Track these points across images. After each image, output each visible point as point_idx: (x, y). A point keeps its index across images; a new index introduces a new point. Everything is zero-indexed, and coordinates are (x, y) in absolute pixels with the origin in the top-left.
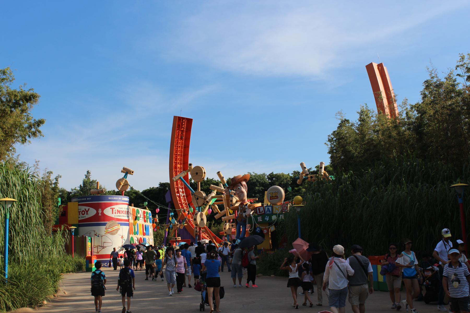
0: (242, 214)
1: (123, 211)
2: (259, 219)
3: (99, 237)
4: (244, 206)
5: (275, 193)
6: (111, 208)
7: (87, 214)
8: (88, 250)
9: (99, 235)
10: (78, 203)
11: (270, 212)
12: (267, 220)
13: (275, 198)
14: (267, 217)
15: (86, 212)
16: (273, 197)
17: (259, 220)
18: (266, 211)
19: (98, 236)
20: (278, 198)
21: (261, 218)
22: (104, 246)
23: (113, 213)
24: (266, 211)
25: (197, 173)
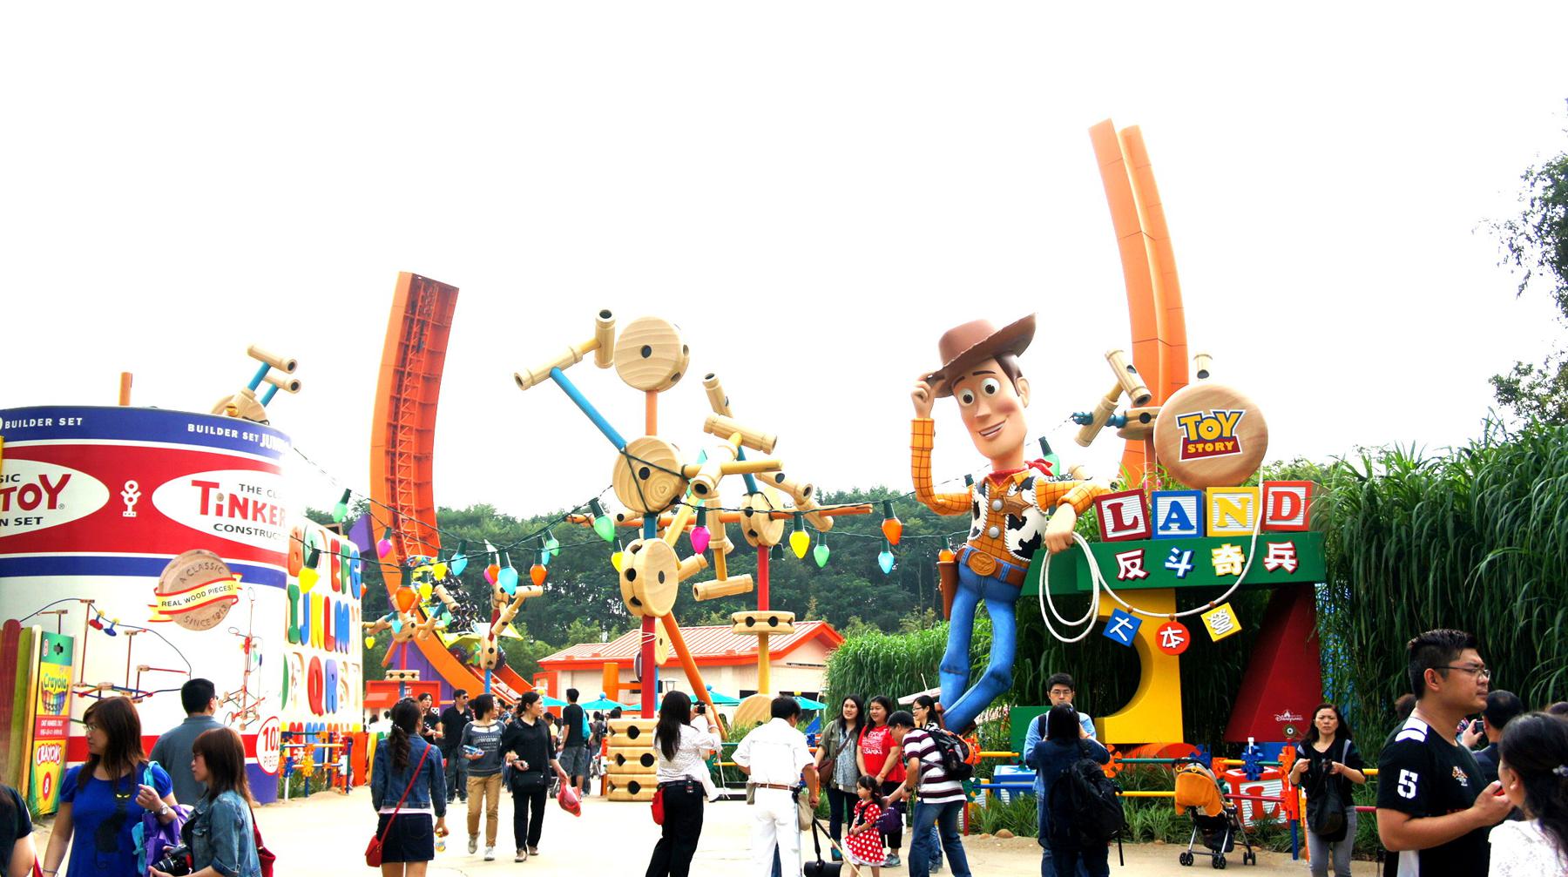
0: (1001, 537)
1: (259, 506)
2: (1123, 565)
3: (114, 634)
4: (1012, 492)
5: (1216, 418)
6: (195, 483)
7: (52, 505)
8: (41, 711)
9: (115, 629)
10: (6, 440)
11: (1185, 524)
12: (1176, 570)
13: (1220, 446)
14: (1179, 557)
15: (45, 496)
16: (1201, 440)
17: (1127, 571)
18: (1161, 522)
19: (110, 632)
20: (1236, 449)
21: (1138, 562)
22: (137, 691)
23: (204, 511)
24: (1161, 522)
25: (646, 351)
